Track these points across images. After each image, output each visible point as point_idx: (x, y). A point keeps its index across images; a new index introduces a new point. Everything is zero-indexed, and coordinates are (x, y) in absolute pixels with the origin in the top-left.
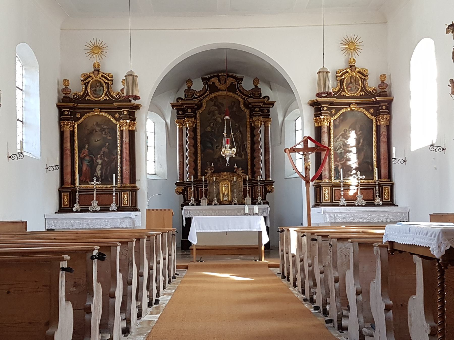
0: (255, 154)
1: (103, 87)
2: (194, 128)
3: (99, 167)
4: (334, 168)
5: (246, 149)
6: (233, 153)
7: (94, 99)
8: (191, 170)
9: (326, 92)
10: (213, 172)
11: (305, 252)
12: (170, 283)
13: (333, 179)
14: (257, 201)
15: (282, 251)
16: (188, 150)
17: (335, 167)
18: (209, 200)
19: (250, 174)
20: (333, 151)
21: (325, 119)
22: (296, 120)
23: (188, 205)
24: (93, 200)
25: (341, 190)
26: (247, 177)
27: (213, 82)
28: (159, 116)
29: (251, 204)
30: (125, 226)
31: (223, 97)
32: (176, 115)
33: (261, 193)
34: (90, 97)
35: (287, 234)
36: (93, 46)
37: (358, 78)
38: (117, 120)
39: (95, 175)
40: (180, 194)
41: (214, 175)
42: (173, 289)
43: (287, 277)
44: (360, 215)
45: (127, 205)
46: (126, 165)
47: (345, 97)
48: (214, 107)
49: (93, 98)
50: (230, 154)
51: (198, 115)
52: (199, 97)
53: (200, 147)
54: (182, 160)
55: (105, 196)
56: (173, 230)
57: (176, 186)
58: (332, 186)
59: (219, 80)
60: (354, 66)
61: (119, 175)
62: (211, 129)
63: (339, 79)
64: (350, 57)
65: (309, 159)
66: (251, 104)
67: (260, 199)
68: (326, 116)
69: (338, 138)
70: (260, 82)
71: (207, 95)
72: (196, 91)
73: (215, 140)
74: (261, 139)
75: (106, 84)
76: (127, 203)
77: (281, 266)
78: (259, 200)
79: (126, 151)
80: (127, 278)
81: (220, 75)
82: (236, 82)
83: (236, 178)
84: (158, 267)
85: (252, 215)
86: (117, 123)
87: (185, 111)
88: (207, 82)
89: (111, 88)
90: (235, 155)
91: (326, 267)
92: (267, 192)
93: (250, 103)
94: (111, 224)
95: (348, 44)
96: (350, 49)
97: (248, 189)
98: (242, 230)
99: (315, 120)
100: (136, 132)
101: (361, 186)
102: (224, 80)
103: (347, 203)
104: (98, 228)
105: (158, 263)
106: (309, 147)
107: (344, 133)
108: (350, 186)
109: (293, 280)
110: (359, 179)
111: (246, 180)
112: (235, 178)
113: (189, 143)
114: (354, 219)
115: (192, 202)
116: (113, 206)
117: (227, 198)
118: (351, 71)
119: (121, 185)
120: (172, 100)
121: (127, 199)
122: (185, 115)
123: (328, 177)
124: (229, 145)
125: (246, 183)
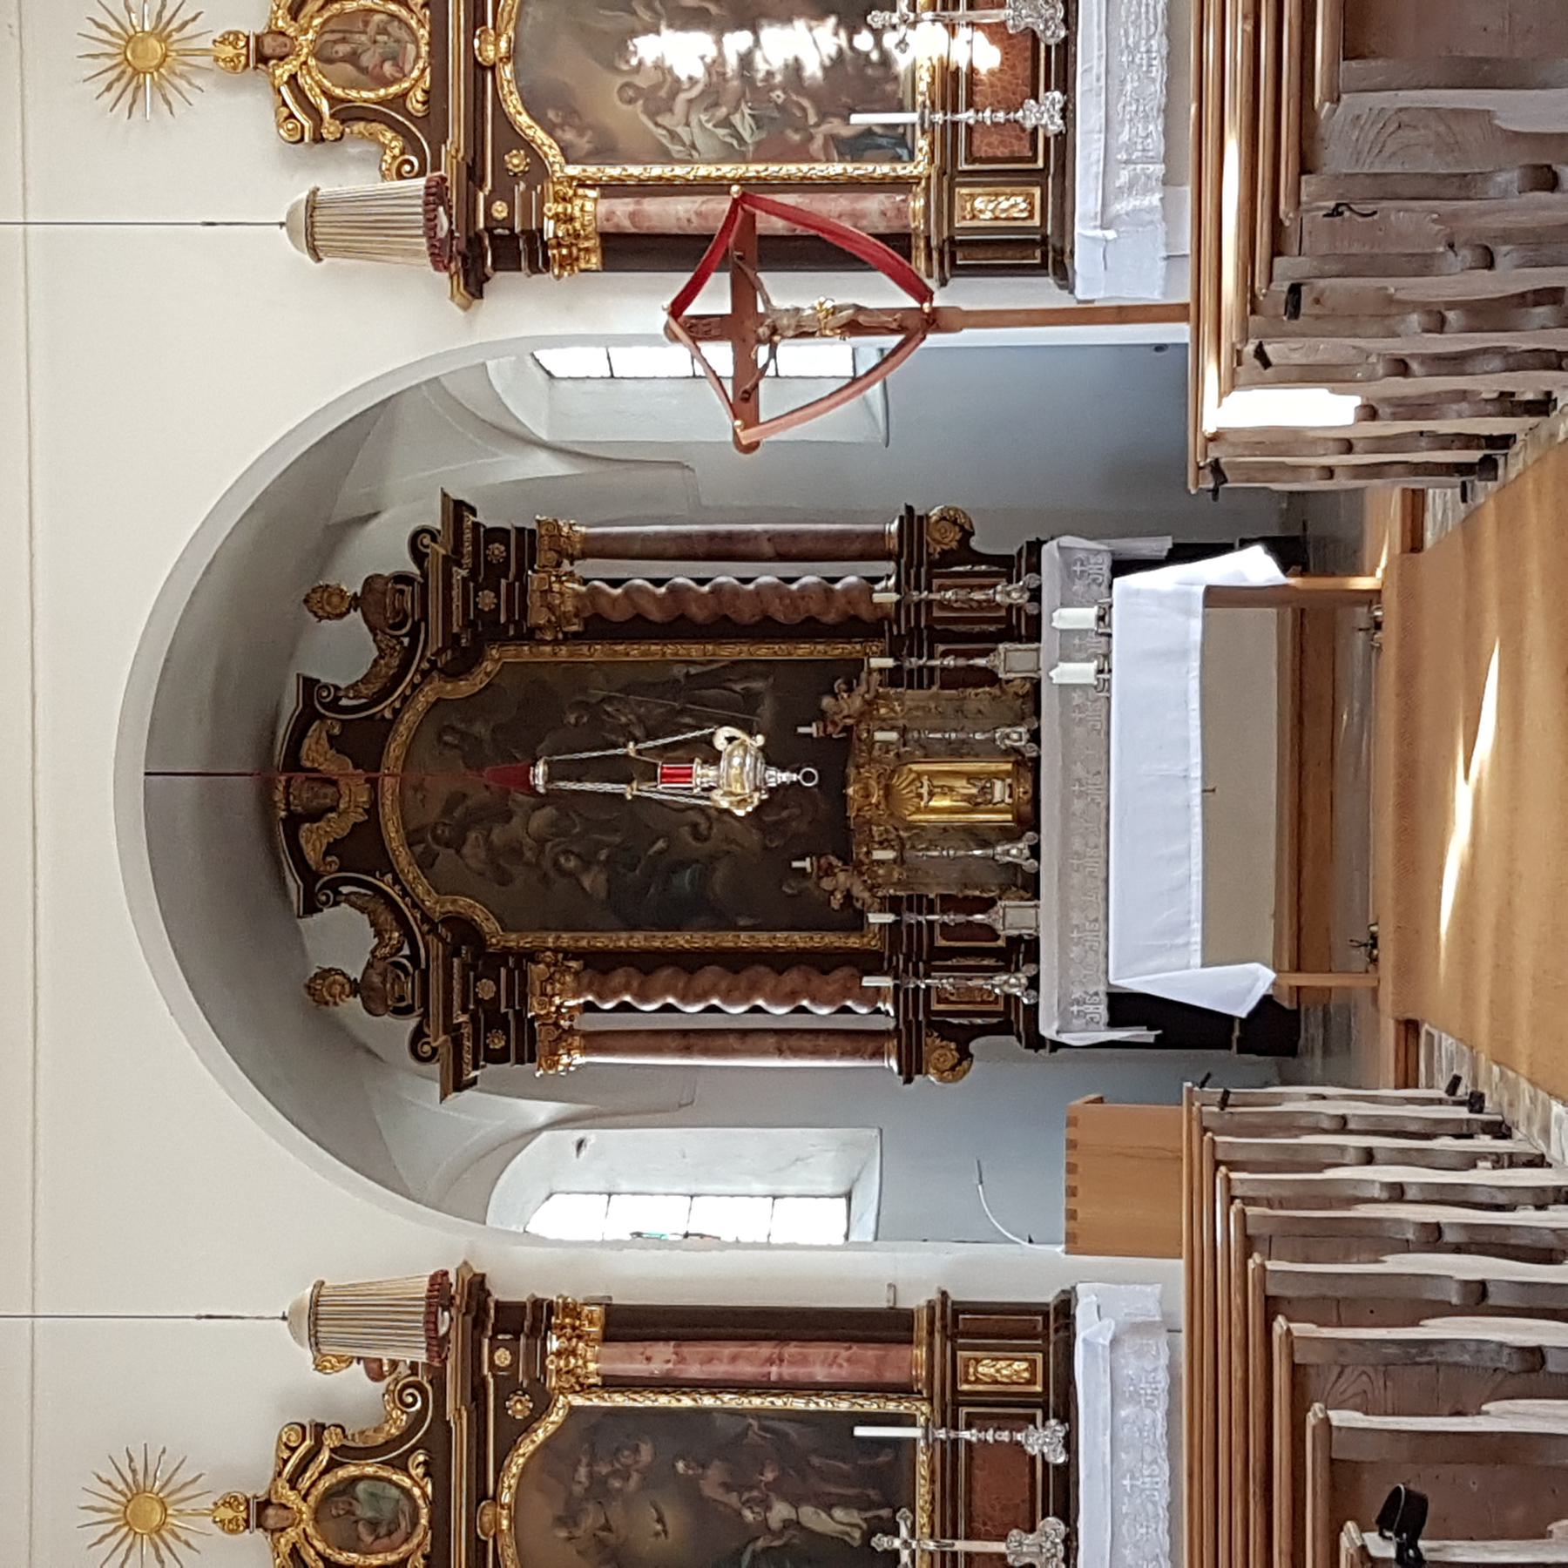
0: (747, 615)
1: (355, 1480)
2: (586, 967)
3: (811, 1517)
4: (840, 161)
5: (715, 666)
6: (743, 744)
7: (422, 1536)
8: (830, 989)
9: (426, 212)
10: (846, 858)
11: (1354, 348)
12: (1509, 1129)
13: (910, 168)
14: (1020, 608)
15: (1329, 472)
16: (715, 1002)
17: (836, 157)
18: (1004, 890)
19: (858, 647)
20: (743, 167)
21: (560, 209)
22: (548, 373)
23: (1033, 1010)
24: (1002, 1557)
25: (971, 122)
26: (876, 662)
27: (327, 853)
28: (510, 1167)
29: (1034, 646)
30: (1163, 1378)
31: (409, 793)
32: (507, 1065)
33: (972, 588)
34: (411, 1553)
35: (1233, 445)
36: (126, 1529)
37: (326, 14)
38: (543, 1405)
39: (856, 1544)
40: (965, 1055)
41: (862, 857)
42: (1547, 1110)
43: (1488, 447)
44: (1123, 13)
45: (1033, 1363)
46: (804, 1361)
47: (436, 95)
48: (466, 850)
49: (415, 1541)
50: (748, 760)
51: (513, 940)
52: (408, 934)
53: (698, 936)
54: (771, 1041)
55: (978, 1486)
56: (1197, 1104)
57: (917, 1078)
58: (949, 176)
59: (315, 816)
60: (258, 38)
61: (861, 1401)
62: (596, 868)
63: (330, 128)
64: (205, 61)
65: (798, 310)
66: (457, 637)
67: (1009, 594)
68: (541, 203)
69: (673, 135)
70: (332, 583)
71: (397, 888)
72: (373, 952)
73: (660, 844)
74: (658, 582)
75: (341, 1465)
76: (1024, 1365)
77: (1416, 483)
78: (1014, 595)
79: (720, 1360)
80: (1499, 1376)
81: (287, 809)
82: (322, 717)
83: (882, 729)
84: (1419, 1198)
85: (1109, 644)
86: (559, 1405)
87: (489, 1017)
88: (325, 886)
89: (362, 1433)
90: (751, 734)
91: (1452, 234)
92: (964, 553)
93: (451, 640)
94: (1148, 1458)
95: (136, 72)
96: (160, 65)
97: (950, 662)
98: (1195, 704)
99: (561, 267)
100: (615, 1302)
101: (950, 6)
102: (316, 786)
103: (1047, 89)
104: (1172, 1531)
105: (1397, 1193)
106: (726, 309)
107: (640, 102)
108: (952, 67)
109: (1513, 415)
110: (912, 16)
111: (897, 669)
112: (879, 736)
113: (675, 996)
114: (1148, 51)
115: (1018, 986)
116: (1042, 1441)
117: (998, 785)
118: (287, 55)
119: (920, 1392)
120: (425, 1085)
121: (1002, 1364)
122: (511, 1017)
123: (899, 198)
124: (697, 768)
125: (911, 671)
